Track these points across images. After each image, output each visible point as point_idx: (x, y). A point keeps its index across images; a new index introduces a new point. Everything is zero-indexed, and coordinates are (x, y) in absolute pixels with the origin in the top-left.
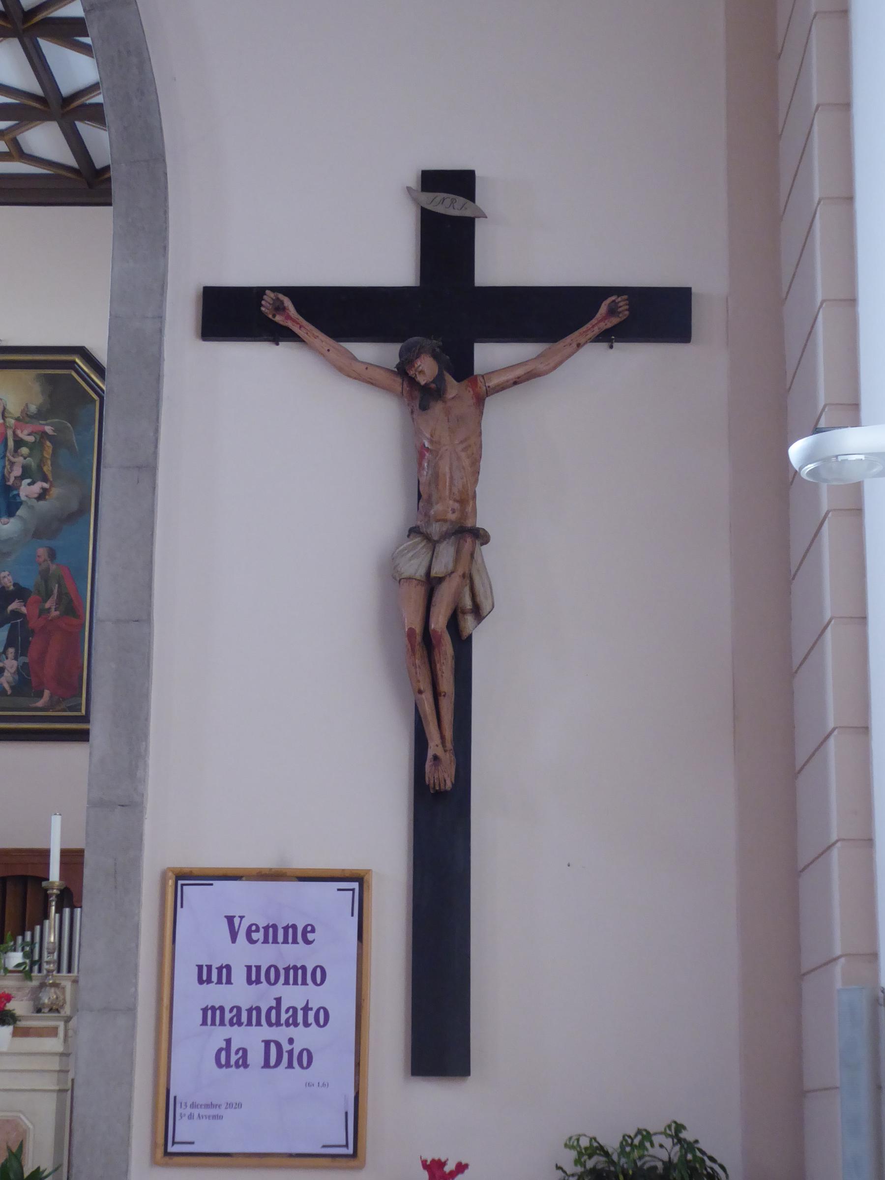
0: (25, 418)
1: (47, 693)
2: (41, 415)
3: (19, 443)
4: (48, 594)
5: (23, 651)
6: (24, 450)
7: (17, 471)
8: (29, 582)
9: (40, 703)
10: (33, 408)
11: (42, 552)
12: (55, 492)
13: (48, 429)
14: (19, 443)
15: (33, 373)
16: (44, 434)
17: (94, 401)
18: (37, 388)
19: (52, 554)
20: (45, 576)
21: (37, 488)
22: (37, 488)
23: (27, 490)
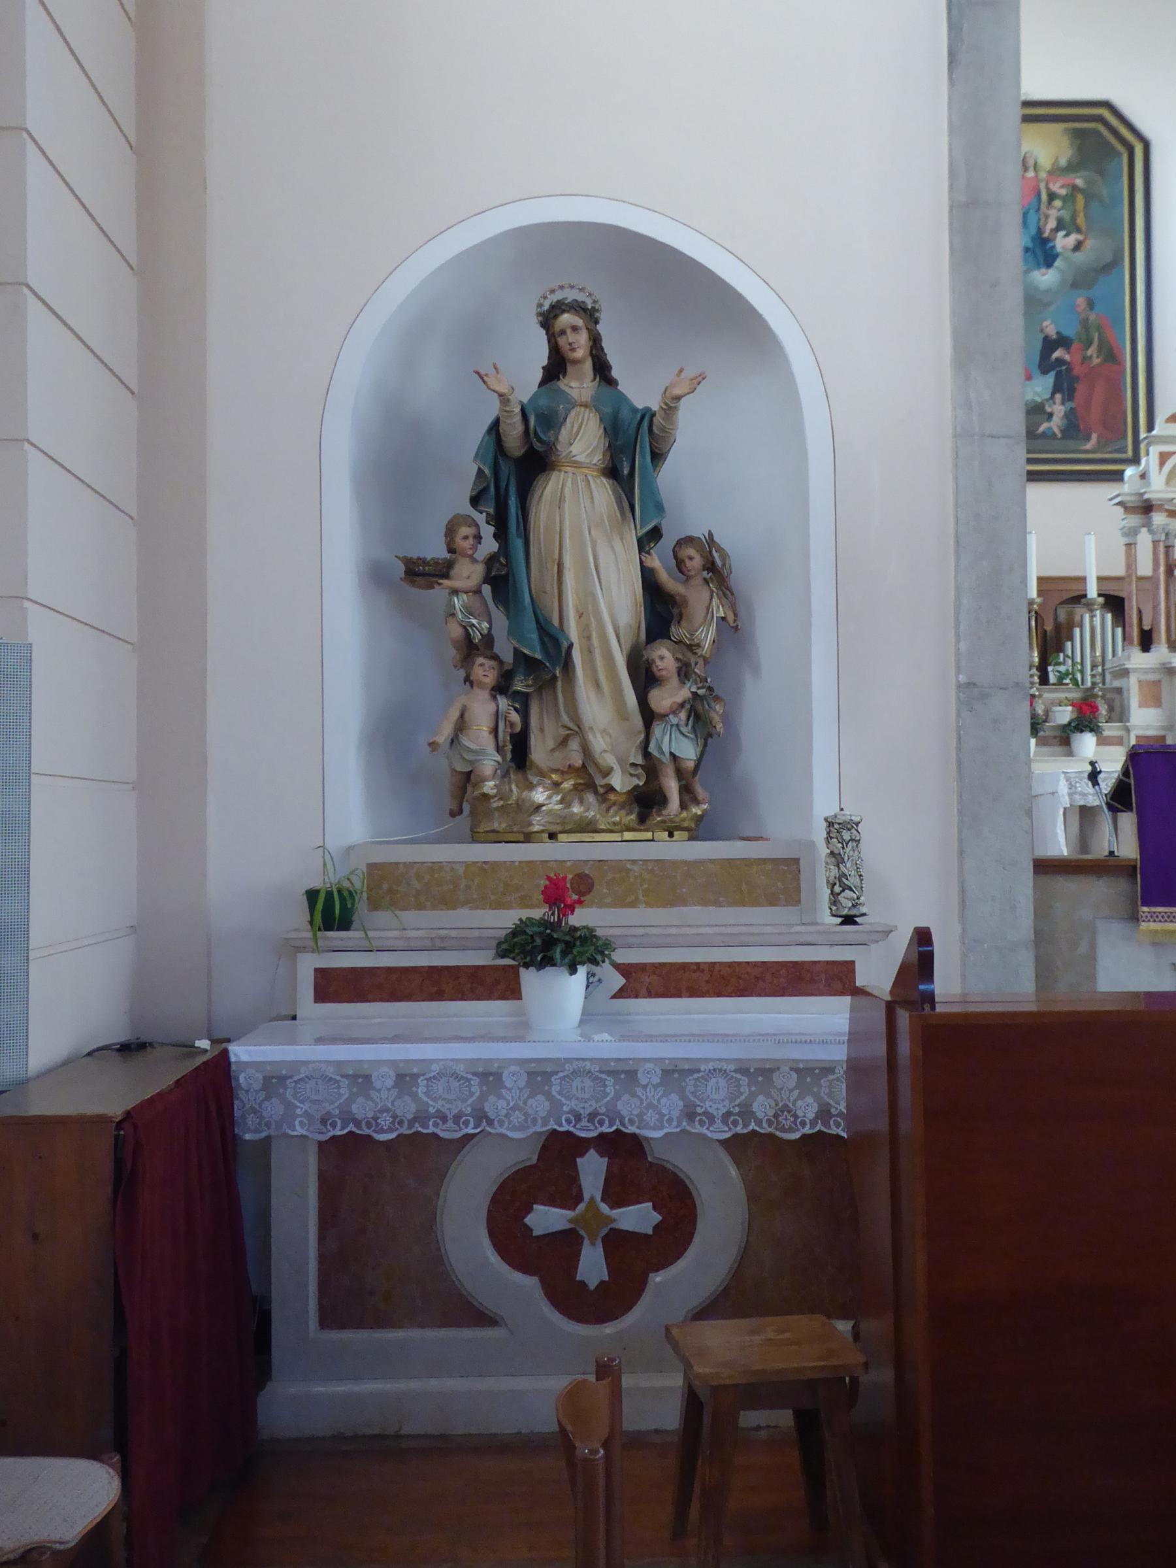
0: (1056, 171)
1: (1094, 436)
2: (1071, 168)
3: (1052, 196)
4: (1089, 344)
5: (1069, 396)
6: (1058, 203)
7: (1052, 224)
8: (1069, 332)
9: (1088, 446)
10: (1063, 162)
11: (1081, 302)
12: (1089, 244)
13: (1079, 182)
14: (1052, 196)
15: (1060, 127)
16: (1075, 188)
17: (1096, 132)
18: (1065, 141)
19: (1091, 304)
20: (1085, 324)
21: (1073, 238)
22: (1073, 238)
23: (1063, 242)
